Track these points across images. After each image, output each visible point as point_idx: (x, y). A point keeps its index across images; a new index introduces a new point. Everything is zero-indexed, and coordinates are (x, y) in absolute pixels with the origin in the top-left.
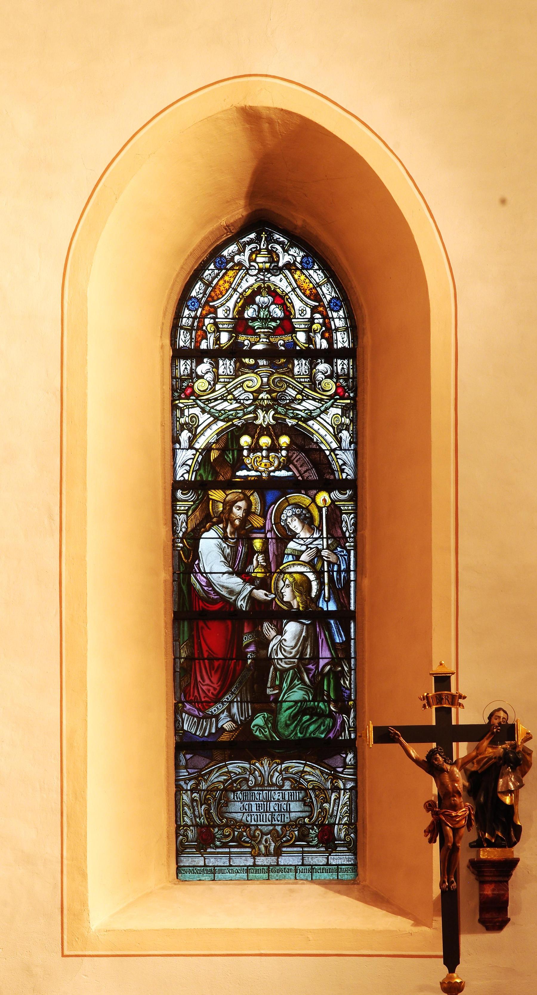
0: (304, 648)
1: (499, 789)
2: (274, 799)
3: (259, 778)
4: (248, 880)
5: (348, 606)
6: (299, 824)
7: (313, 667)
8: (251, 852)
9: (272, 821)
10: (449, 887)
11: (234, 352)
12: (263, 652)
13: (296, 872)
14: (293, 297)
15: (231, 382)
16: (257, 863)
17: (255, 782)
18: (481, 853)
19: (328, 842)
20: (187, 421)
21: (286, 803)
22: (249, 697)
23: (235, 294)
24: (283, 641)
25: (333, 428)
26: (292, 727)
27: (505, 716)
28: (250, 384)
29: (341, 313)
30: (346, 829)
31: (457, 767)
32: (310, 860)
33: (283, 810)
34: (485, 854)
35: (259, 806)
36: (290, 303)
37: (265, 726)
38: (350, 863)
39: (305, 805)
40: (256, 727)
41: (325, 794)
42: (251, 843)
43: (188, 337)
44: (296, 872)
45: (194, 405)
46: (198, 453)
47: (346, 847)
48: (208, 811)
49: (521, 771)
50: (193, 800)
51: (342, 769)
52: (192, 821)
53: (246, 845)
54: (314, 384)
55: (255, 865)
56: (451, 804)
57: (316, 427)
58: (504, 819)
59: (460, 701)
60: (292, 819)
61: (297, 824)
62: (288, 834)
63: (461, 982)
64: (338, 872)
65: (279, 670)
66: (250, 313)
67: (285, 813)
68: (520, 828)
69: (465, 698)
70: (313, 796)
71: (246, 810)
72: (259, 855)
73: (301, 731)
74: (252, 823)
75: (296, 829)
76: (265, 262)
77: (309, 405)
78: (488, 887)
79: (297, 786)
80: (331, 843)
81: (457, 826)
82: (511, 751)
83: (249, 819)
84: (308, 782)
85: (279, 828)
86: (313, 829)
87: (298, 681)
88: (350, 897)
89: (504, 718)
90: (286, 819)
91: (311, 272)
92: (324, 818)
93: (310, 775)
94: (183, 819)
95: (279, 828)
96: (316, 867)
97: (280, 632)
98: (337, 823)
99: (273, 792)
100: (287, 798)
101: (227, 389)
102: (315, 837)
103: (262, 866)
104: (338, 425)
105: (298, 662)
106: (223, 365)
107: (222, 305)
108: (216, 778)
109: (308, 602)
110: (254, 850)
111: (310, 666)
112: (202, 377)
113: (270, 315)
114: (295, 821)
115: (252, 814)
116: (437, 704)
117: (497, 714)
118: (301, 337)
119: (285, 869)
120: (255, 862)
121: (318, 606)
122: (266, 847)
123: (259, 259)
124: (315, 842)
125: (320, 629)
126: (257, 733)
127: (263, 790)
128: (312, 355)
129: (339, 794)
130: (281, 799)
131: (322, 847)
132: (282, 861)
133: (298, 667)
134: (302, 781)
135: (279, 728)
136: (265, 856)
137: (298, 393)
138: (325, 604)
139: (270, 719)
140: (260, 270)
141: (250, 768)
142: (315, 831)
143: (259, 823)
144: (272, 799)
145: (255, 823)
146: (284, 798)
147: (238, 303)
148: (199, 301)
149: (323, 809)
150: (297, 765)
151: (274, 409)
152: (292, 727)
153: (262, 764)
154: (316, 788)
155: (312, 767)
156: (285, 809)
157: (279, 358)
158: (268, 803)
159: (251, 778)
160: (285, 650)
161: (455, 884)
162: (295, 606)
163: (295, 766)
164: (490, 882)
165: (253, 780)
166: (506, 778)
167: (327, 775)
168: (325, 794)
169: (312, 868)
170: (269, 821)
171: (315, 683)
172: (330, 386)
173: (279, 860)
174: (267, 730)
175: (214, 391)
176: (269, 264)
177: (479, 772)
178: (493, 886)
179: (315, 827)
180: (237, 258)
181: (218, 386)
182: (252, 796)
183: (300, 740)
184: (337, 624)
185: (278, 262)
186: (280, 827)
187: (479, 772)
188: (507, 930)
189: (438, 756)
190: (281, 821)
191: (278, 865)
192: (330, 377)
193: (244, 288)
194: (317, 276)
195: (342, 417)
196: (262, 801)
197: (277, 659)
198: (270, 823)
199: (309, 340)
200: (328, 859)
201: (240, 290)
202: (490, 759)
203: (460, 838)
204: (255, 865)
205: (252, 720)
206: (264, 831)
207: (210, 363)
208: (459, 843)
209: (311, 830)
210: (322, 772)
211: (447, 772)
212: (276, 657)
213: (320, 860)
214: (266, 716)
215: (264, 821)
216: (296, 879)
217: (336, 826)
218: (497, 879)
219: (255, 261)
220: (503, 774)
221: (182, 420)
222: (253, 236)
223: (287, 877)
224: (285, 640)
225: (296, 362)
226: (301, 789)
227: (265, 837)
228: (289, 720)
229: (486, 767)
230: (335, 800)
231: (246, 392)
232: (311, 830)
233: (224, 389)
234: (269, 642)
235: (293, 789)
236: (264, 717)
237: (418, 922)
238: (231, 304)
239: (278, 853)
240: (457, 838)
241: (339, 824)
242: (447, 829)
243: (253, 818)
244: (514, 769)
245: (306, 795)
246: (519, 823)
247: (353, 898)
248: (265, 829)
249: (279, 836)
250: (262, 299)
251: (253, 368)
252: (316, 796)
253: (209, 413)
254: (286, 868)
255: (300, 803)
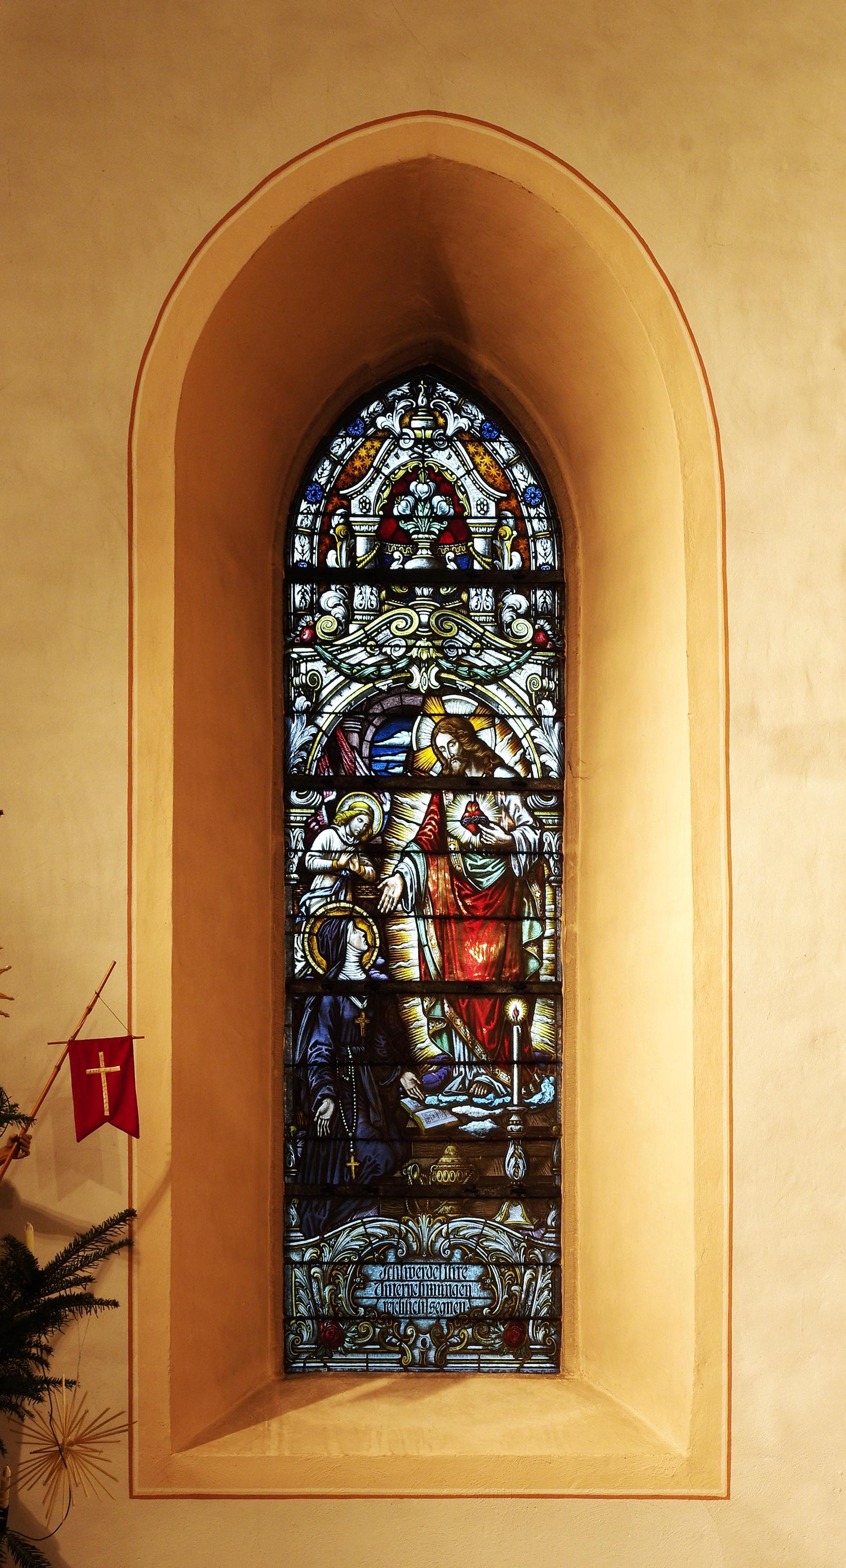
8: (400, 1359)
11: (377, 574)
14: (468, 483)
15: (373, 620)
20: (304, 681)
23: (378, 479)
25: (530, 696)
28: (401, 624)
29: (542, 510)
36: (463, 493)
43: (307, 547)
45: (315, 656)
46: (321, 733)
48: (335, 1293)
50: (310, 1277)
52: (309, 1311)
53: (392, 1349)
54: (501, 629)
57: (501, 694)
66: (401, 508)
76: (425, 429)
77: (492, 658)
91: (496, 445)
94: (297, 1308)
101: (365, 632)
104: (536, 692)
106: (361, 593)
107: (358, 493)
108: (348, 1238)
112: (329, 613)
113: (432, 512)
118: (480, 545)
123: (415, 424)
128: (500, 582)
134: (479, 1250)
137: (475, 641)
140: (418, 441)
147: (383, 492)
148: (322, 488)
150: (472, 1225)
151: (438, 665)
157: (449, 581)
172: (524, 629)
175: (347, 634)
176: (431, 432)
180: (381, 422)
181: (353, 628)
185: (445, 427)
192: (526, 616)
193: (392, 467)
194: (505, 451)
195: (542, 678)
199: (494, 552)
201: (386, 471)
207: (341, 591)
219: (409, 426)
221: (297, 680)
222: (405, 388)
225: (473, 592)
227: (422, 1336)
230: (530, 1281)
231: (395, 636)
233: (362, 632)
238: (371, 494)
241: (534, 1319)
250: (420, 486)
251: (407, 599)
252: (502, 1274)
253: (338, 668)
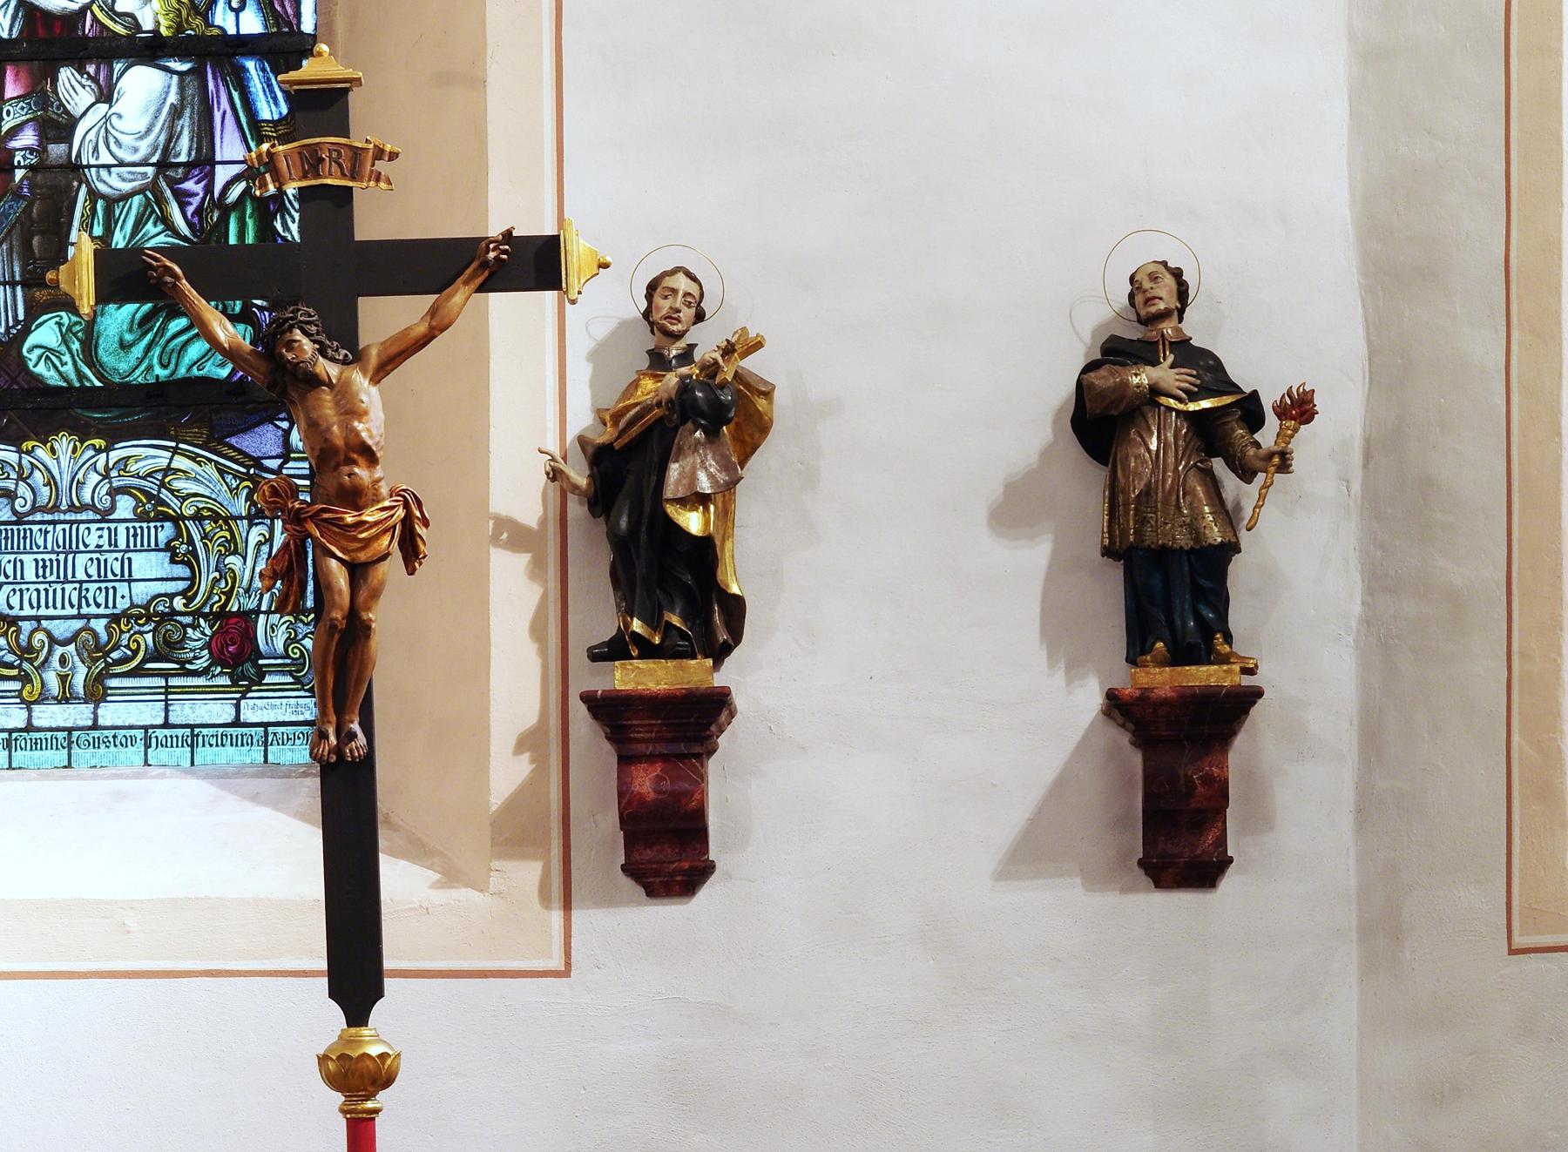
0: (173, 137)
1: (670, 491)
2: (86, 546)
3: (45, 491)
4: (10, 767)
5: (295, 22)
6: (156, 614)
7: (198, 188)
8: (20, 691)
9: (80, 607)
10: (338, 750)
12: (56, 150)
13: (147, 746)
16: (36, 723)
17: (34, 501)
18: (618, 674)
19: (237, 656)
21: (119, 555)
22: (17, 269)
24: (114, 118)
26: (138, 351)
27: (693, 288)
30: (291, 626)
31: (364, 371)
32: (187, 710)
33: (110, 577)
34: (629, 677)
35: (44, 567)
37: (63, 349)
38: (301, 718)
39: (173, 561)
40: (38, 352)
41: (230, 530)
42: (19, 667)
44: (147, 746)
47: (290, 673)
49: (738, 438)
51: (279, 461)
55: (30, 727)
56: (341, 486)
58: (688, 579)
59: (381, 166)
60: (137, 601)
61: (153, 614)
62: (125, 642)
63: (383, 1056)
64: (266, 744)
65: (103, 197)
67: (117, 585)
68: (739, 602)
69: (393, 156)
70: (196, 537)
71: (7, 577)
72: (43, 699)
73: (165, 362)
74: (22, 613)
75: (147, 628)
78: (642, 773)
79: (153, 510)
80: (248, 665)
81: (363, 556)
82: (701, 383)
83: (15, 601)
84: (184, 498)
85: (99, 626)
86: (195, 627)
87: (155, 225)
88: (280, 810)
89: (687, 294)
90: (118, 599)
92: (229, 595)
93: (188, 479)
95: (99, 626)
96: (205, 731)
97: (106, 95)
98: (264, 608)
99: (82, 527)
100: (122, 545)
102: (202, 649)
103: (51, 729)
105: (156, 176)
109: (184, 13)
110: (28, 687)
111: (189, 185)
114: (146, 607)
115: (24, 587)
116: (304, 177)
117: (669, 282)
119: (115, 737)
120: (30, 717)
121: (209, 25)
122: (63, 679)
124: (201, 664)
125: (217, 86)
126: (41, 369)
127: (54, 523)
129: (271, 530)
130: (106, 547)
131: (221, 673)
132: (108, 716)
133: (154, 186)
134: (165, 494)
135: (101, 352)
136: (59, 703)
138: (232, 15)
139: (78, 328)
141: (20, 464)
142: (203, 633)
143: (43, 612)
144: (82, 547)
145: (33, 612)
146: (113, 543)
149: (223, 572)
150: (152, 452)
152: (138, 351)
153: (53, 451)
154: (205, 513)
155: (193, 458)
156: (118, 571)
158: (70, 557)
159: (23, 489)
160: (117, 142)
161: (361, 739)
162: (148, 25)
163: (146, 456)
164: (651, 759)
165: (29, 496)
166: (690, 460)
167: (235, 477)
168: (230, 530)
169: (194, 734)
170: (72, 606)
171: (202, 230)
173: (100, 712)
174: (67, 358)
177: (617, 446)
178: (657, 769)
179: (202, 621)
182: (25, 538)
183: (159, 384)
184: (263, 70)
186: (104, 622)
187: (617, 446)
188: (708, 892)
189: (298, 335)
190: (107, 607)
191: (95, 726)
196: (53, 552)
197: (98, 167)
198: (74, 612)
200: (238, 707)
202: (647, 409)
203: (375, 594)
204: (30, 727)
205: (26, 332)
206: (56, 633)
208: (368, 609)
209: (189, 630)
210: (222, 471)
211: (330, 385)
212: (93, 162)
213: (222, 711)
214: (66, 321)
215: (59, 605)
216: (146, 763)
217: (262, 618)
218: (661, 748)
220: (680, 450)
223: (122, 757)
224: (120, 116)
226: (166, 517)
227: (59, 651)
228: (130, 330)
229: (635, 431)
230: (259, 544)
232: (189, 630)
234: (73, 122)
235: (142, 517)
236: (60, 324)
237: (451, 877)
239: (96, 693)
240: (363, 595)
242: (328, 568)
243: (26, 598)
244: (713, 434)
245: (179, 535)
246: (735, 589)
247: (288, 814)
248: (61, 629)
249: (98, 648)
254: (119, 735)
255: (162, 554)
